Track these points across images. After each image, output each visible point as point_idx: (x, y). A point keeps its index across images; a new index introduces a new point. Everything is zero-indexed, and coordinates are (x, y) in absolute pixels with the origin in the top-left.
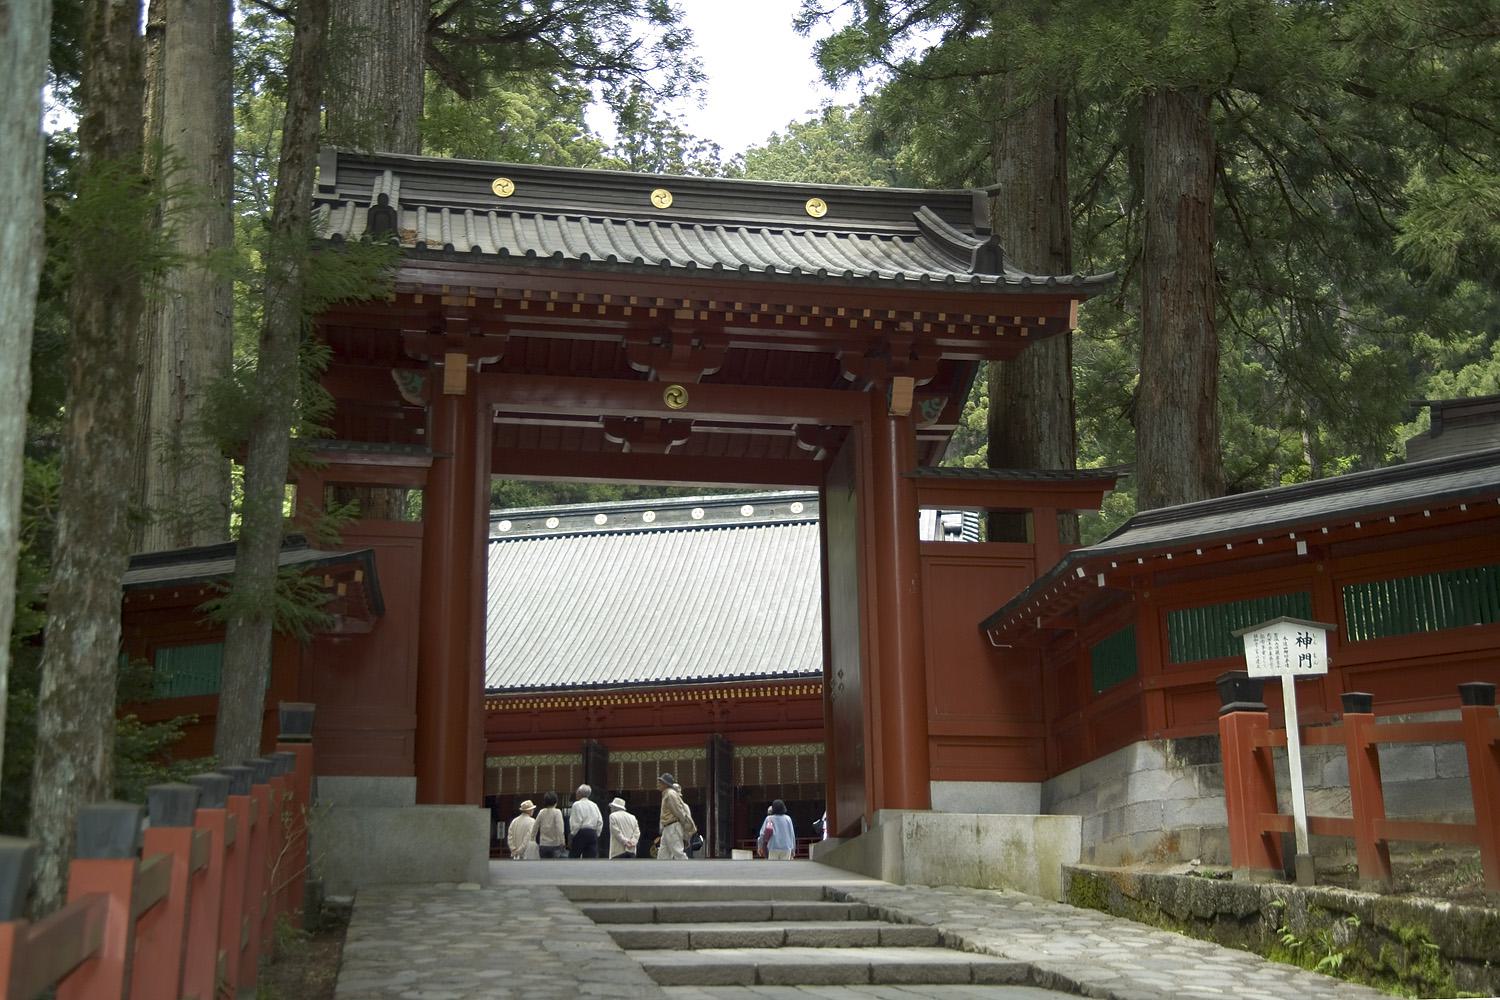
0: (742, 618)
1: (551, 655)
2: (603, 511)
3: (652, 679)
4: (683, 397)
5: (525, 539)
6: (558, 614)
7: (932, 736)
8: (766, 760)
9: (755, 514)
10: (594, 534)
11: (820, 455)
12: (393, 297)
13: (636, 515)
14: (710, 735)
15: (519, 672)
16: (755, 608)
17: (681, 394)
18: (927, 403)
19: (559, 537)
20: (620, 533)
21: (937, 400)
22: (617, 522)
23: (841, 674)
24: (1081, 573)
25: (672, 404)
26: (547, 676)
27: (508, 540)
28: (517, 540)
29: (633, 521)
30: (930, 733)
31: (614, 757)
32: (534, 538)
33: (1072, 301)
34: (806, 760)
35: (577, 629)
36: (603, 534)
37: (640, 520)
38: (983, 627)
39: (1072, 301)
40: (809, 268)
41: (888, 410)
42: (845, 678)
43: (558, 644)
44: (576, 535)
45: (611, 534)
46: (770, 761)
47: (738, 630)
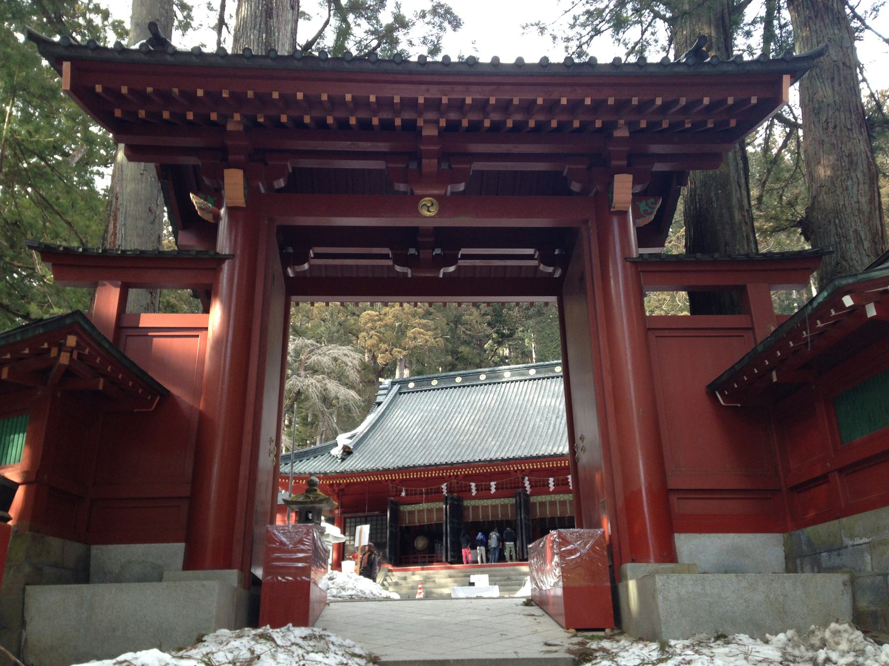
0: (531, 426)
1: (431, 448)
2: (460, 375)
3: (483, 459)
4: (434, 207)
5: (421, 391)
6: (436, 427)
7: (670, 490)
8: (420, 511)
9: (537, 373)
10: (455, 387)
11: (557, 274)
12: (758, 640)
13: (476, 377)
14: (855, 543)
15: (413, 458)
16: (538, 420)
17: (432, 205)
18: (644, 202)
19: (438, 389)
20: (468, 386)
21: (652, 200)
22: (466, 381)
23: (582, 438)
24: (848, 301)
25: (425, 213)
26: (427, 459)
27: (413, 392)
28: (417, 392)
29: (474, 380)
30: (672, 485)
31: (402, 508)
32: (425, 391)
33: (784, 76)
34: (504, 506)
35: (445, 435)
36: (460, 387)
37: (478, 379)
38: (712, 389)
39: (784, 76)
40: (532, 58)
41: (610, 207)
42: (585, 441)
43: (435, 442)
44: (446, 388)
45: (464, 386)
46: (485, 508)
47: (529, 431)
